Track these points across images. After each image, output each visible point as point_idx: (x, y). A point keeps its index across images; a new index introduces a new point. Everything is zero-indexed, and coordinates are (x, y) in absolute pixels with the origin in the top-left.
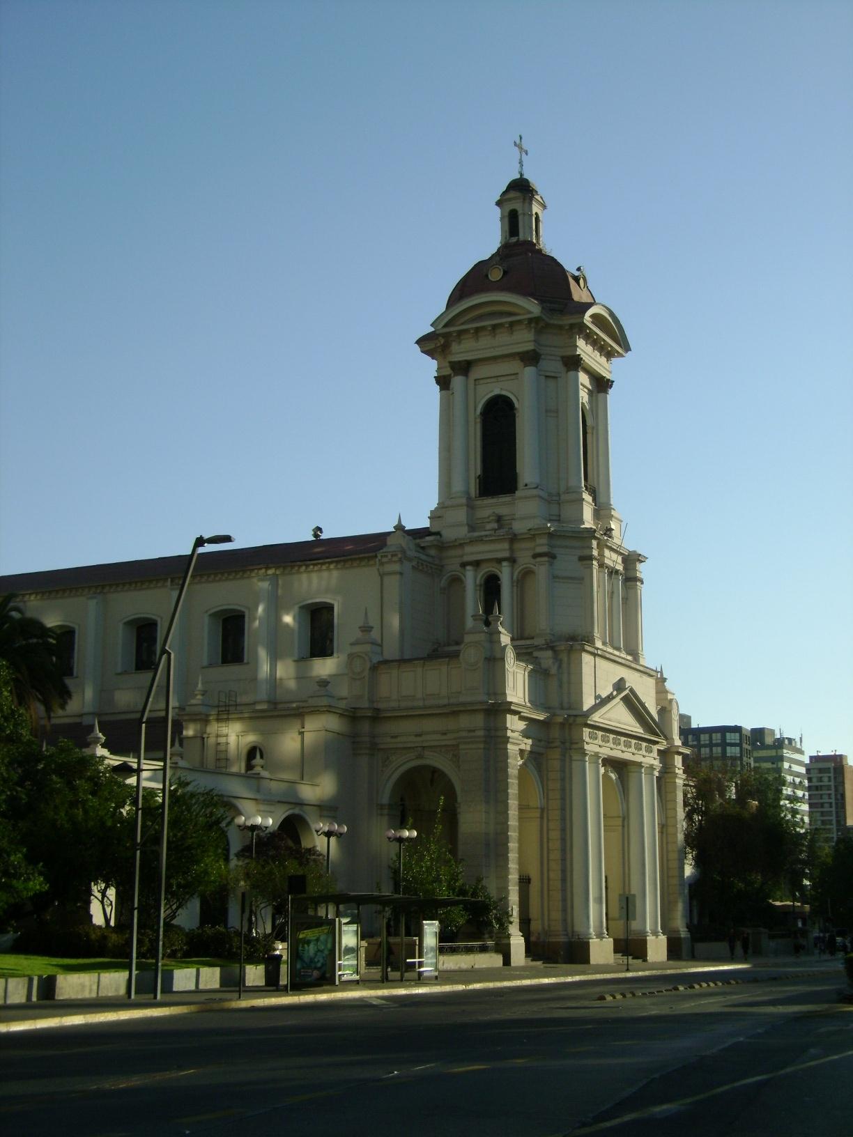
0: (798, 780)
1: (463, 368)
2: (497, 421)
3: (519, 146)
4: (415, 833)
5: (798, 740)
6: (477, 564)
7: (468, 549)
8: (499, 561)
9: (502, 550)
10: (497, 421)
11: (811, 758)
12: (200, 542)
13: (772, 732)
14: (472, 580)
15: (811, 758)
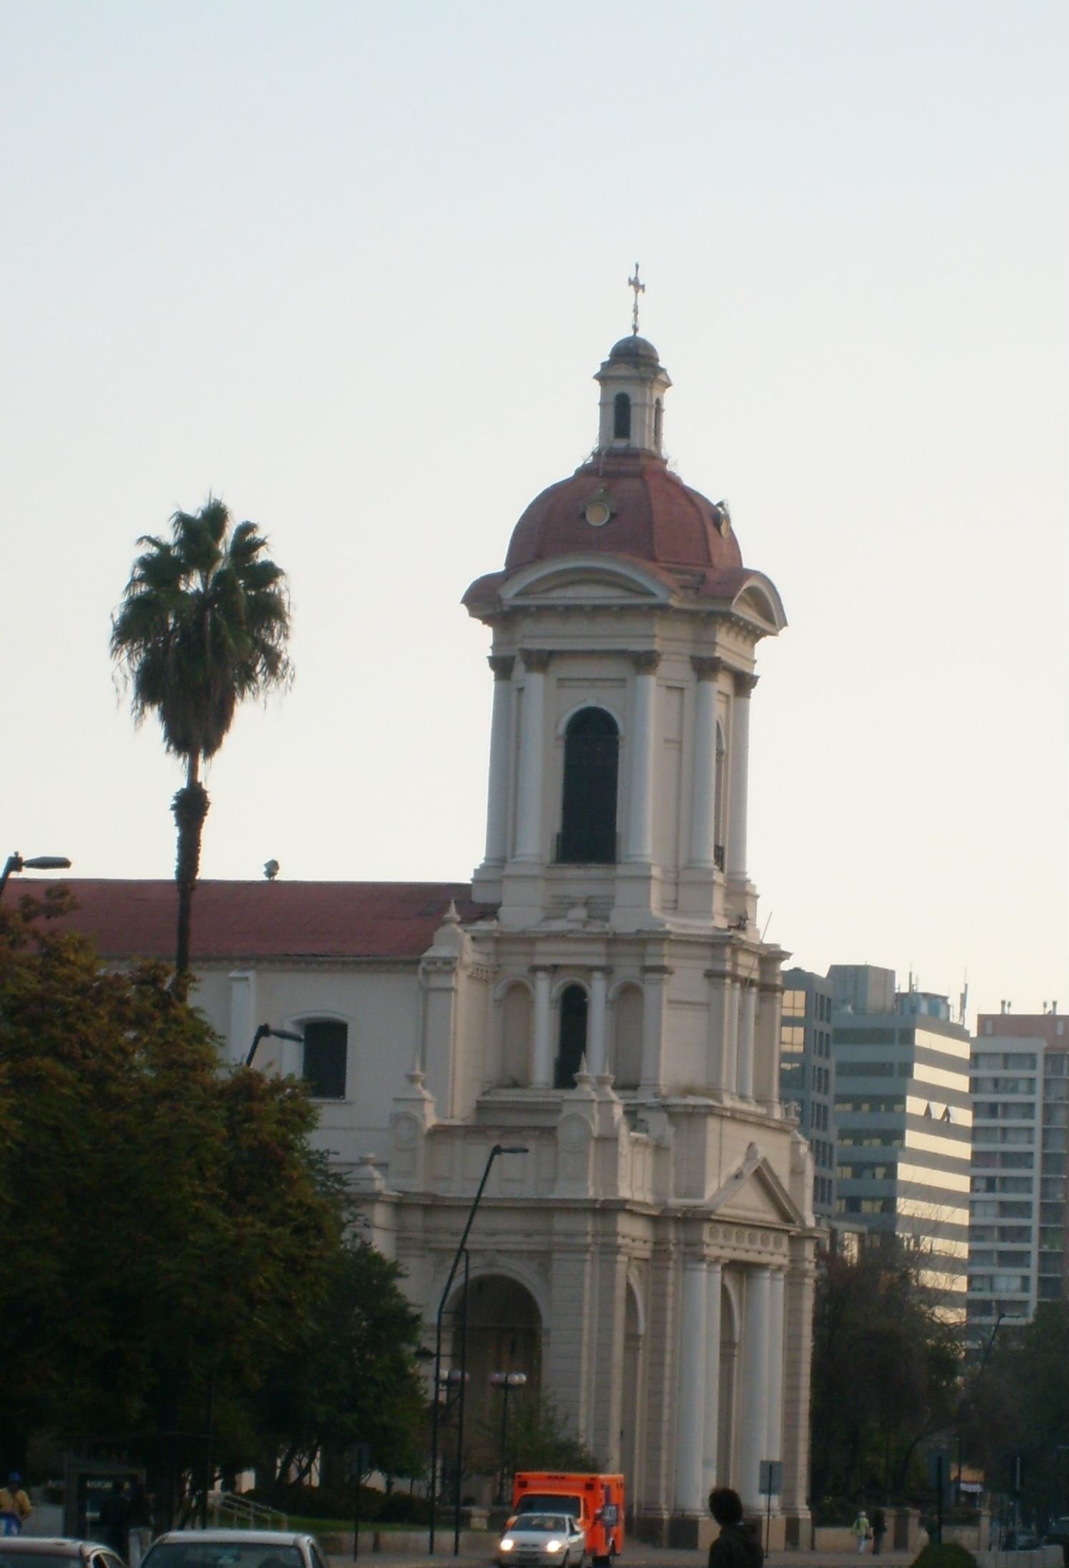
0: (938, 1110)
1: (540, 661)
2: (592, 752)
3: (636, 284)
4: (524, 1378)
5: (954, 1001)
6: (554, 969)
7: (540, 947)
8: (590, 970)
9: (595, 956)
10: (592, 752)
11: (983, 1020)
12: (15, 863)
13: (888, 976)
14: (545, 993)
15: (983, 1020)
